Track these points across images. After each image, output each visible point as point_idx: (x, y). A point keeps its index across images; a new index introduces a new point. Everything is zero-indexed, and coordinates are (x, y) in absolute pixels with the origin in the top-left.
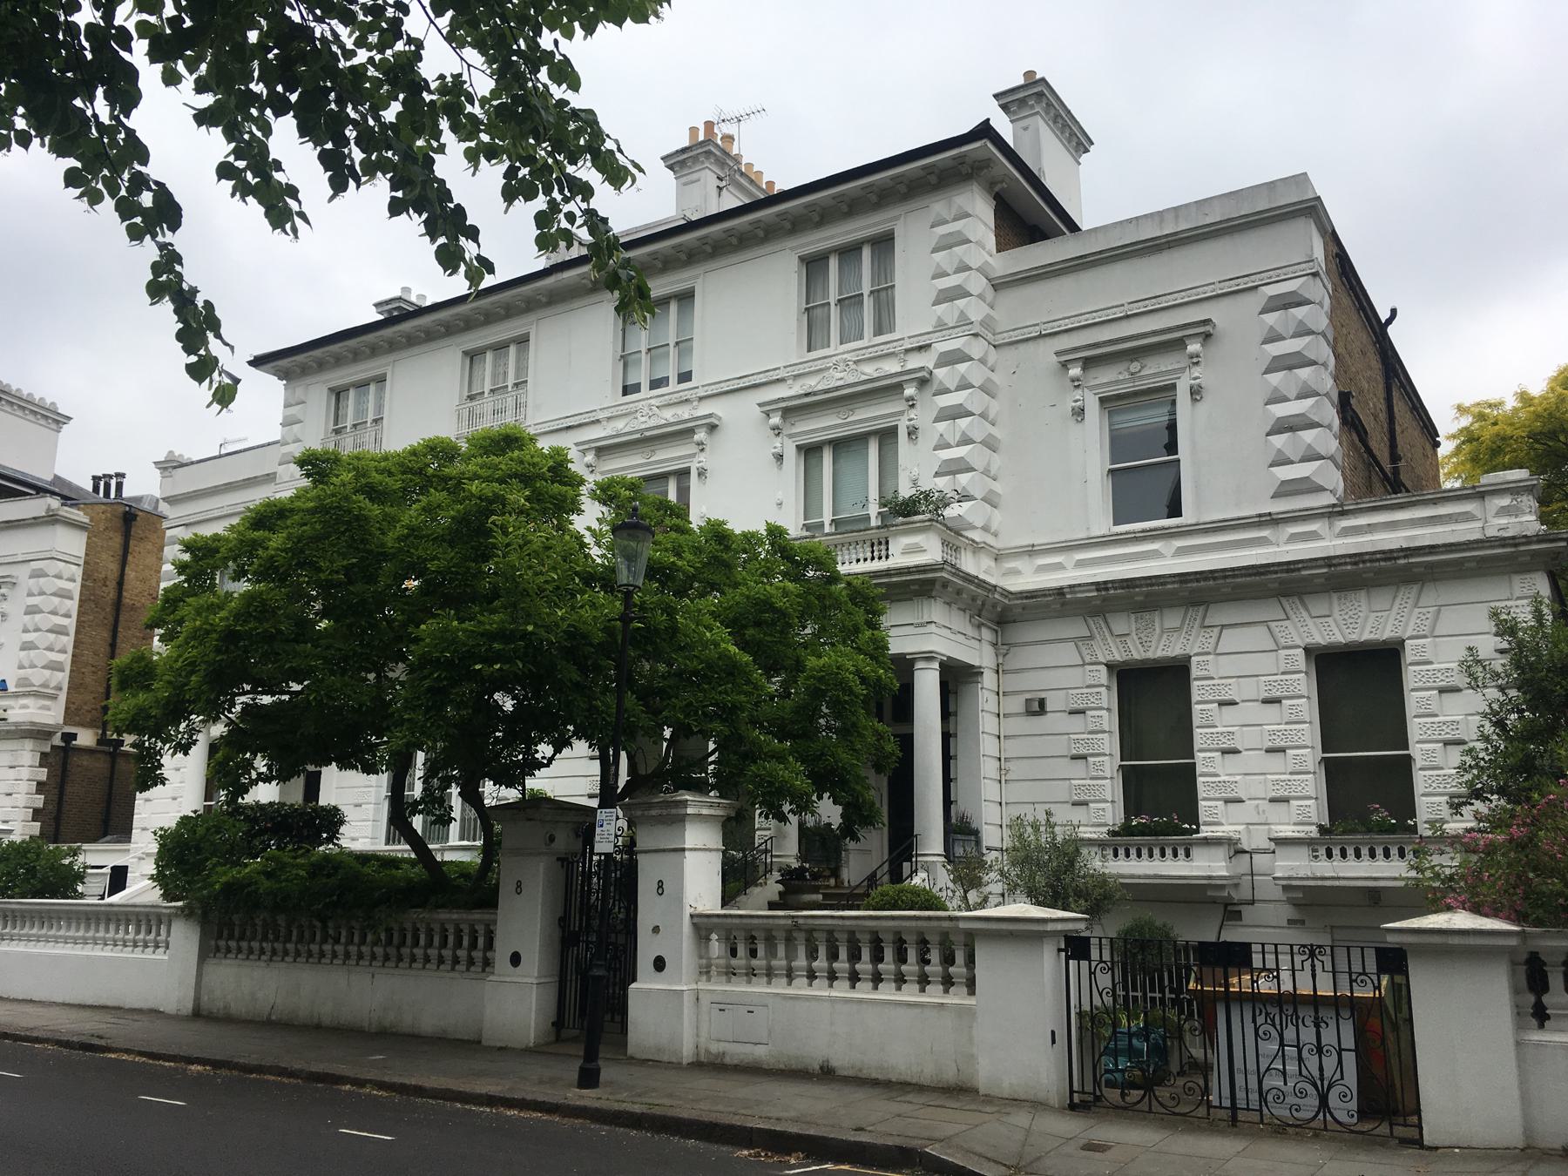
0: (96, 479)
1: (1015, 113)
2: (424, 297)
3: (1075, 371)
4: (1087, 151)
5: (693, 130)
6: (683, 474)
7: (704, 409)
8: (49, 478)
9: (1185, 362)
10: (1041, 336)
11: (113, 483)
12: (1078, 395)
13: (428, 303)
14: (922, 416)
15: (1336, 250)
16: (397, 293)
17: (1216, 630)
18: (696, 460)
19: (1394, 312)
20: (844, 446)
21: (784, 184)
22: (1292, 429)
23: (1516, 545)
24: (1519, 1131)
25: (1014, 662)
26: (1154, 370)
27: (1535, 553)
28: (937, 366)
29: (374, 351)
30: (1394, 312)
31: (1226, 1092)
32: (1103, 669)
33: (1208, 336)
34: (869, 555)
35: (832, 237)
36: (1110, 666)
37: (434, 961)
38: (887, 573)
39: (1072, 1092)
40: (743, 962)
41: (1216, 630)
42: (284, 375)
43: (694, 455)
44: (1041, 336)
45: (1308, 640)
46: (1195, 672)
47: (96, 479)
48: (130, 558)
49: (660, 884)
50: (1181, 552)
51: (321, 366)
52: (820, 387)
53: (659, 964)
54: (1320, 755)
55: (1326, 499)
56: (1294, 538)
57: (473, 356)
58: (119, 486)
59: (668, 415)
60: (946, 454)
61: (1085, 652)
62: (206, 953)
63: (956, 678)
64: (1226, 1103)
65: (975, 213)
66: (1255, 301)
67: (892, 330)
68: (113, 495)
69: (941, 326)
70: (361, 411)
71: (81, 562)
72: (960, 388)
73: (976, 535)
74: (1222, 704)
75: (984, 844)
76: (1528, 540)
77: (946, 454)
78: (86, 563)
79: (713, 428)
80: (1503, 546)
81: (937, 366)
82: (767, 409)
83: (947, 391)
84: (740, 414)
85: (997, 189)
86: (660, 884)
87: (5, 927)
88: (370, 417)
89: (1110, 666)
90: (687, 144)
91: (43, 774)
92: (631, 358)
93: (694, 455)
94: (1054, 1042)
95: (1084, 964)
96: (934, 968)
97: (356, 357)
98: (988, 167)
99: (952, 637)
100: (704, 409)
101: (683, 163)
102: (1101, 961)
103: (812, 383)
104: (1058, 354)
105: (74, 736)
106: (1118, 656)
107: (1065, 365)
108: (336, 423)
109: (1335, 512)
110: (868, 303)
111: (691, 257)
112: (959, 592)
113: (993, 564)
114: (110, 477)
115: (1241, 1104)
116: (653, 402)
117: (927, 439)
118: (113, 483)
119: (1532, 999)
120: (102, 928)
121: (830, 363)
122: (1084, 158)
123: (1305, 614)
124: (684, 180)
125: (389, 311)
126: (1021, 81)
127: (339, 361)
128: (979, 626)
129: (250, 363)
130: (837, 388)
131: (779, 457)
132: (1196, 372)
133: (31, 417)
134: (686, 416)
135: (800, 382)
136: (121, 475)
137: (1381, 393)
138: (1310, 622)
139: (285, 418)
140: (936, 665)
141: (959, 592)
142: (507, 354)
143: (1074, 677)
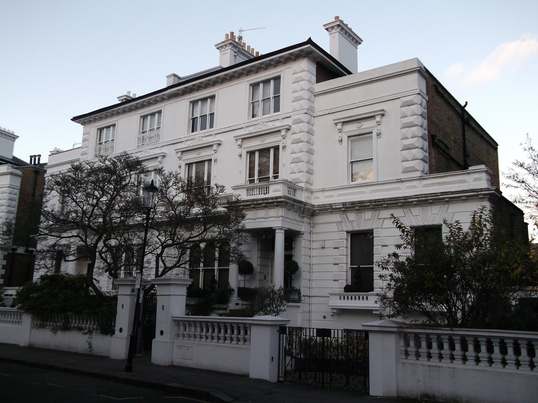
0: (31, 157)
1: (330, 31)
2: (135, 95)
3: (339, 126)
4: (360, 44)
5: (227, 35)
6: (210, 160)
7: (218, 137)
8: (11, 158)
9: (212, 152)
10: (329, 114)
11: (37, 158)
12: (340, 135)
13: (137, 97)
14: (288, 141)
15: (431, 82)
16: (126, 94)
17: (382, 220)
18: (214, 156)
19: (466, 103)
20: (264, 152)
21: (262, 53)
22: (409, 149)
23: (477, 192)
24: (395, 390)
25: (316, 230)
26: (366, 125)
27: (485, 195)
28: (293, 124)
29: (112, 115)
30: (466, 103)
31: (325, 377)
32: (345, 233)
33: (383, 115)
34: (258, 192)
35: (256, 79)
36: (348, 232)
37: (242, 340)
38: (267, 199)
39: (279, 377)
40: (193, 333)
41: (382, 220)
42: (84, 124)
43: (213, 154)
44: (329, 114)
45: (347, 229)
46: (375, 235)
47: (31, 157)
48: (37, 186)
49: (123, 306)
50: (372, 192)
51: (95, 120)
52: (254, 131)
53: (162, 333)
54: (349, 266)
55: (418, 174)
56: (408, 188)
57: (144, 117)
58: (39, 159)
59: (271, 125)
60: (294, 156)
61: (339, 227)
62: (33, 326)
63: (291, 237)
64: (321, 381)
65: (304, 68)
66: (398, 103)
67: (279, 111)
68: (33, 163)
69: (294, 110)
70: (107, 137)
71: (19, 188)
72: (300, 132)
73: (302, 185)
74: (383, 246)
75: (302, 294)
76: (481, 190)
77: (294, 156)
78: (21, 188)
79: (219, 145)
80: (474, 192)
81: (293, 124)
82: (237, 138)
83: (295, 133)
84: (228, 139)
85: (317, 61)
86: (123, 306)
87: (2, 317)
88: (110, 139)
89: (348, 232)
90: (224, 40)
91: (4, 262)
92: (256, 104)
93: (213, 154)
94: (272, 360)
95: (285, 335)
96: (435, 349)
97: (107, 117)
98: (311, 53)
99: (291, 221)
100: (218, 137)
101: (222, 47)
102: (334, 337)
103: (252, 130)
104: (334, 120)
105: (16, 249)
106: (350, 229)
107: (336, 124)
108: (100, 141)
109: (421, 179)
110: (272, 101)
111: (215, 83)
112: (293, 205)
113: (310, 195)
114: (36, 156)
115: (325, 381)
116: (200, 135)
117: (289, 150)
118: (37, 158)
119: (404, 349)
120: (9, 317)
121: (259, 122)
122: (359, 46)
123: (411, 215)
124: (222, 53)
125: (122, 100)
126: (334, 20)
127: (101, 118)
128: (303, 217)
129: (75, 119)
130: (204, 144)
131: (241, 156)
132: (379, 127)
133: (4, 136)
134: (211, 140)
135: (248, 129)
136: (40, 156)
137: (460, 131)
138: (412, 217)
139: (83, 139)
140: (283, 232)
141: (293, 205)
142: (110, 130)
143: (336, 236)
